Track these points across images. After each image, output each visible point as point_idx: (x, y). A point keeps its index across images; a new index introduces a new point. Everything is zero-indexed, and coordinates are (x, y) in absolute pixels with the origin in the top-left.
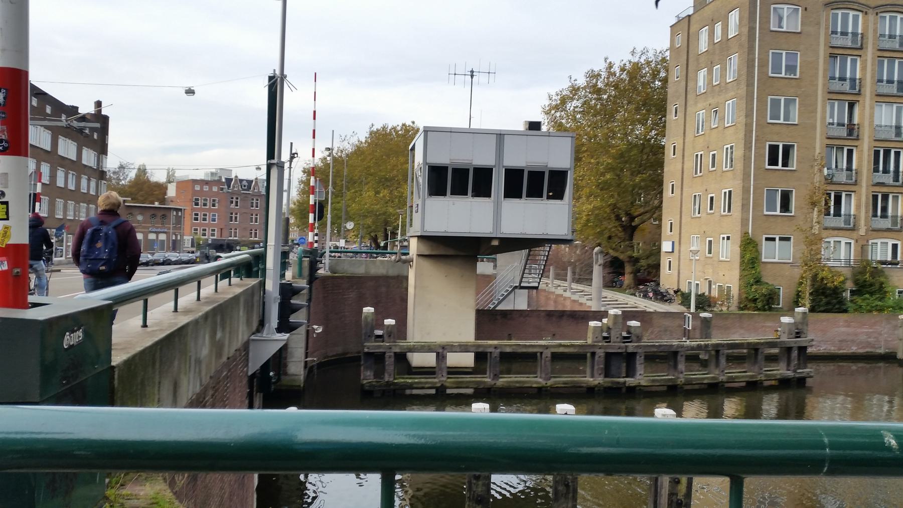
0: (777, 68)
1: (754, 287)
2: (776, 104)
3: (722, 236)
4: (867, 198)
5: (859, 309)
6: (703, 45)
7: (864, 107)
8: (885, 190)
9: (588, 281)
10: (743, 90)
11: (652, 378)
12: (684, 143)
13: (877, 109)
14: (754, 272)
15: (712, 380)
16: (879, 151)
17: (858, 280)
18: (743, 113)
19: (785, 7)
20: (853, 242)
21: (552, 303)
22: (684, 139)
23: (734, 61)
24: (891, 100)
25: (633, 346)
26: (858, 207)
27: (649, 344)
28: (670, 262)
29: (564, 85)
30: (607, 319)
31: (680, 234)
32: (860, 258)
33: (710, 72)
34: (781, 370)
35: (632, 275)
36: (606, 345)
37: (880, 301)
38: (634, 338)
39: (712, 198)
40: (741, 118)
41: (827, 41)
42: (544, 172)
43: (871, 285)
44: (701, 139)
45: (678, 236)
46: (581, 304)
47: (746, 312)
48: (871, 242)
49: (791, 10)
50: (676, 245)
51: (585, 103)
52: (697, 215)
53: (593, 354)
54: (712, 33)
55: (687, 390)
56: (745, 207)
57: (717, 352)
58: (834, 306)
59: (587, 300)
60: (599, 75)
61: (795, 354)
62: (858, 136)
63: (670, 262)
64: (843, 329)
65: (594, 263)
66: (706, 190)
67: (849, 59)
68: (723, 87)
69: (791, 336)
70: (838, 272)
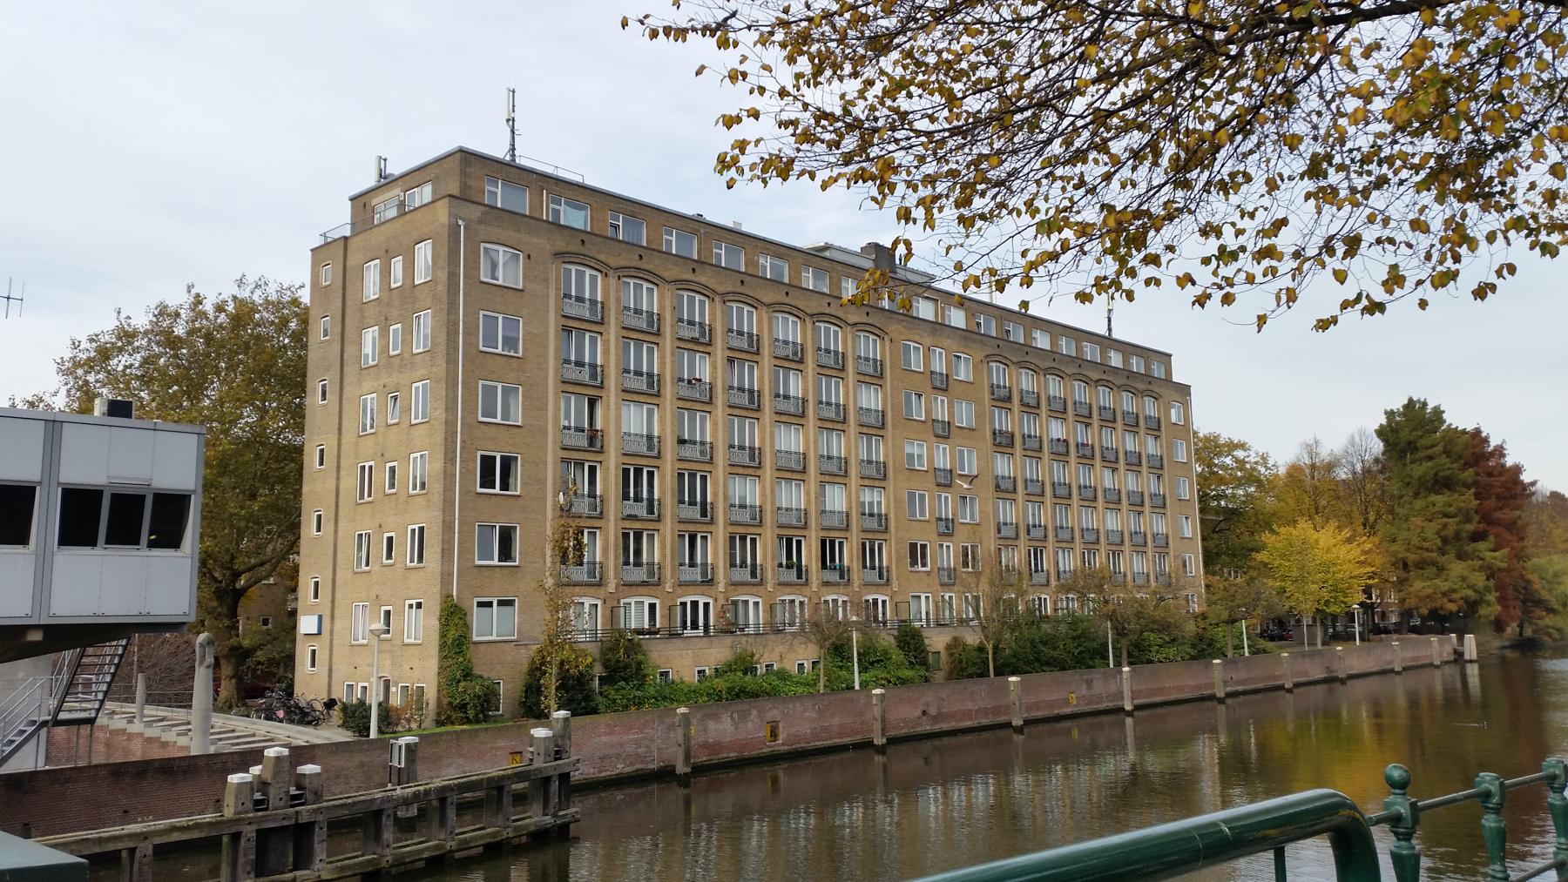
0: (491, 340)
1: (462, 684)
2: (490, 393)
3: (408, 602)
4: (616, 538)
5: (612, 706)
6: (372, 288)
7: (609, 406)
8: (638, 525)
9: (184, 701)
10: (441, 368)
11: (339, 864)
12: (339, 445)
13: (624, 410)
14: (461, 659)
15: (435, 850)
16: (629, 469)
17: (609, 660)
18: (441, 404)
19: (501, 249)
20: (599, 602)
21: (101, 748)
22: (339, 440)
23: (426, 322)
24: (641, 398)
25: (308, 811)
26: (605, 551)
27: (336, 803)
28: (314, 652)
29: (105, 325)
30: (260, 767)
31: (333, 601)
32: (609, 627)
33: (384, 333)
34: (535, 818)
35: (233, 681)
36: (262, 816)
37: (638, 690)
38: (309, 796)
39: (390, 540)
40: (438, 411)
41: (559, 309)
42: (145, 496)
43: (626, 667)
44: (370, 442)
45: (330, 605)
46: (165, 745)
47: (449, 728)
48: (622, 601)
49: (509, 255)
51: (145, 361)
52: (364, 568)
53: (236, 837)
54: (386, 272)
55: (459, 860)
56: (446, 553)
57: (443, 801)
58: (579, 704)
59: (179, 735)
60: (178, 315)
61: (555, 786)
62: (602, 447)
63: (314, 652)
64: (604, 739)
65: (197, 663)
66: (380, 526)
67: (587, 335)
68: (406, 361)
69: (548, 759)
70: (584, 651)
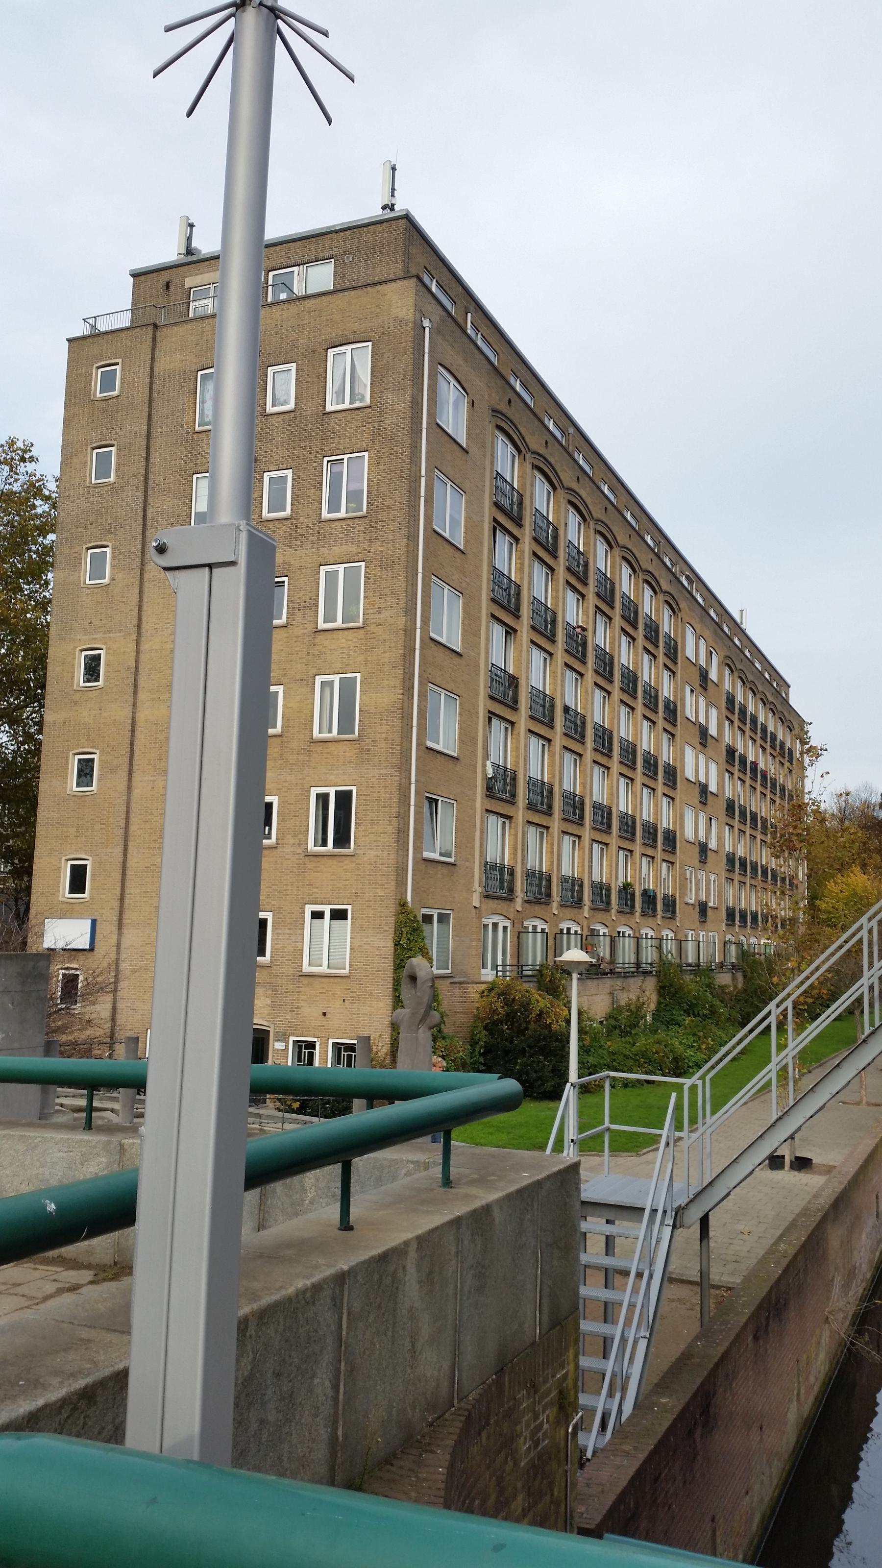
50: (107, 929)
